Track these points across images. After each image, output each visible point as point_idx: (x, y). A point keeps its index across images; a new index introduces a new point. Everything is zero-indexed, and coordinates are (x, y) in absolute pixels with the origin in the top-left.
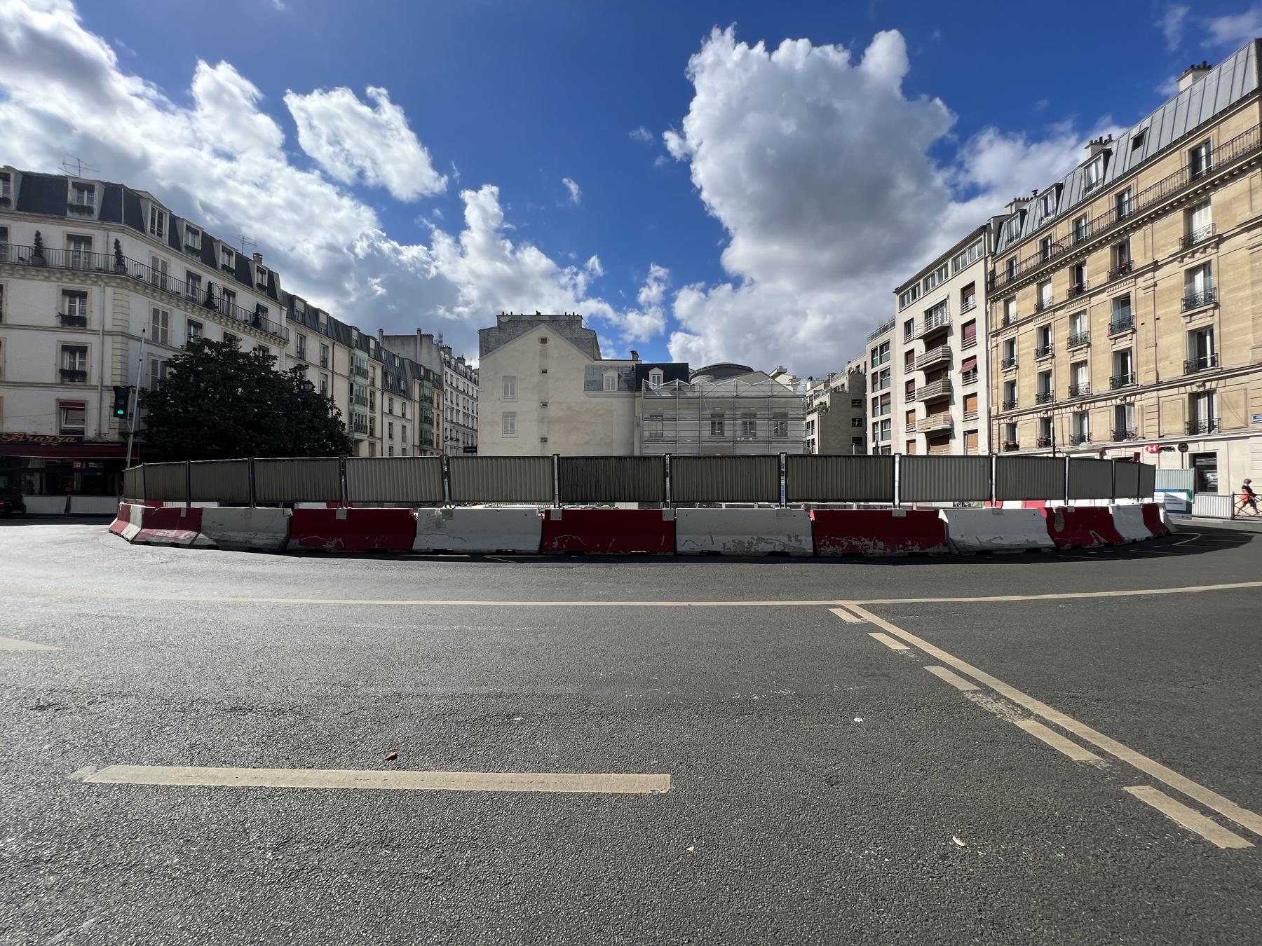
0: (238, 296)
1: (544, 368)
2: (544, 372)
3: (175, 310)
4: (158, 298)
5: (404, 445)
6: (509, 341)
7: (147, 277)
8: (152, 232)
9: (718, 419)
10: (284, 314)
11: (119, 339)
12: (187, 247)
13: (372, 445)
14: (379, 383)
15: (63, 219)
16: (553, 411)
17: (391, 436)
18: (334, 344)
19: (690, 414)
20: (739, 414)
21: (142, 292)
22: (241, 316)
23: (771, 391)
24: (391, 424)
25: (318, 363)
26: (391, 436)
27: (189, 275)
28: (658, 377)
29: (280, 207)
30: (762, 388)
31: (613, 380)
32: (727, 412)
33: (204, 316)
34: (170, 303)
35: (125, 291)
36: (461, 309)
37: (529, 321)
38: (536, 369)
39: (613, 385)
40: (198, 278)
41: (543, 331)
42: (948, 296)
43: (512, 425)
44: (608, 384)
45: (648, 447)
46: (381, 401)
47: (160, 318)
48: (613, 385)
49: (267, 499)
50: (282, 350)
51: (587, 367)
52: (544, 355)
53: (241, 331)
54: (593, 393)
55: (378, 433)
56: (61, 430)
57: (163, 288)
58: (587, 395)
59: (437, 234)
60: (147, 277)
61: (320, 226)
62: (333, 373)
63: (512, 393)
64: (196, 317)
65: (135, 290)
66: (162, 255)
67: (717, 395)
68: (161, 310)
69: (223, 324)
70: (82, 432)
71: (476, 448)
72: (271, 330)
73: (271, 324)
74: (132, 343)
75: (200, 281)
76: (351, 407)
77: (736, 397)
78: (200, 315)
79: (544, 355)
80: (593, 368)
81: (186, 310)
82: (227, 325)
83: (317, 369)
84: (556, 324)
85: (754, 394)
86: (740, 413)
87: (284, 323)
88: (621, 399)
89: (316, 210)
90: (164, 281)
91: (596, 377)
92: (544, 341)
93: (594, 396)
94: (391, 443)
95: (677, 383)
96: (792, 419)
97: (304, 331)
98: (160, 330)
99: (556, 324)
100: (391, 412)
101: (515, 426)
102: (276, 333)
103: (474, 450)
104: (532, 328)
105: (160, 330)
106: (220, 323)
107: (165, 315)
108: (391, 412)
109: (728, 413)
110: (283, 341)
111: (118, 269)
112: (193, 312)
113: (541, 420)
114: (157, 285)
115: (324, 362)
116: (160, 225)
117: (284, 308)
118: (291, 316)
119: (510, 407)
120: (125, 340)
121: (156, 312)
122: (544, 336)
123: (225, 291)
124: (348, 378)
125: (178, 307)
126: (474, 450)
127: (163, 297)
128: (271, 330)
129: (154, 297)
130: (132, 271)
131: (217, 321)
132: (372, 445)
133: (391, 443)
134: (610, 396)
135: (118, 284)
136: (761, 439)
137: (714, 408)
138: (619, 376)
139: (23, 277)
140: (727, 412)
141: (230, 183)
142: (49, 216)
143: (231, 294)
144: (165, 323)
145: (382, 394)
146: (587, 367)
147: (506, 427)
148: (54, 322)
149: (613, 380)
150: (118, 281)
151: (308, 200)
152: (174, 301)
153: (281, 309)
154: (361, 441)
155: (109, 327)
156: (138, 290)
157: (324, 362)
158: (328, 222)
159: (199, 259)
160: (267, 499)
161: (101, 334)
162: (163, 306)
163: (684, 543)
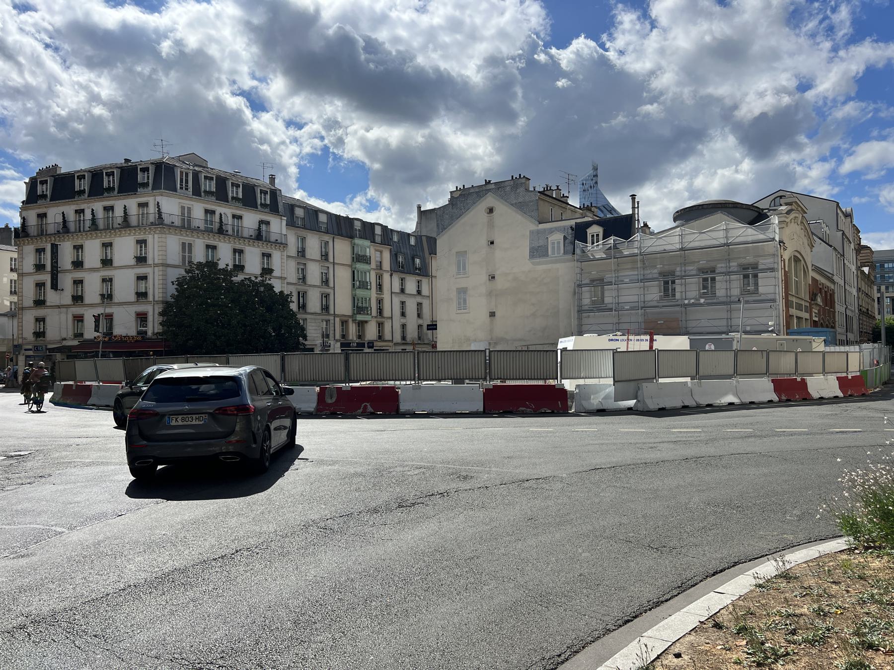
0: (244, 218)
1: (491, 240)
2: (492, 243)
3: (197, 240)
4: (184, 235)
5: (420, 322)
6: (461, 216)
7: (178, 222)
8: (181, 188)
9: (670, 279)
10: (284, 223)
11: (161, 268)
12: (205, 192)
13: (380, 325)
14: (386, 265)
15: (136, 194)
16: (501, 283)
17: (403, 314)
18: (334, 238)
19: (628, 274)
20: (693, 269)
21: (173, 233)
22: (246, 234)
23: (726, 237)
24: (403, 303)
25: (318, 257)
26: (403, 314)
27: (207, 211)
28: (598, 235)
29: (441, 27)
30: (714, 235)
31: (559, 243)
32: (719, 266)
33: (217, 240)
34: (192, 236)
35: (164, 236)
36: (649, 108)
37: (477, 192)
38: (484, 242)
39: (559, 248)
40: (213, 212)
41: (490, 200)
42: (595, 169)
43: (465, 300)
44: (553, 248)
45: (589, 317)
46: (391, 283)
47: (187, 248)
48: (559, 248)
49: (304, 380)
50: (283, 253)
51: (532, 232)
52: (491, 225)
53: (247, 245)
54: (538, 260)
55: (387, 312)
56: (138, 332)
57: (189, 228)
58: (533, 264)
59: (611, 14)
60: (178, 222)
61: (482, 39)
62: (334, 263)
63: (464, 269)
64: (212, 242)
65: (170, 233)
66: (187, 203)
67: (658, 249)
68: (187, 243)
69: (232, 242)
70: (146, 332)
71: (436, 325)
72: (273, 239)
73: (272, 234)
74: (169, 270)
75: (215, 214)
76: (354, 292)
77: (682, 249)
78: (215, 240)
79: (491, 225)
80: (538, 232)
81: (204, 238)
82: (235, 243)
83: (317, 264)
84: (501, 192)
85: (703, 244)
86: (735, 264)
87: (284, 231)
88: (568, 264)
89: (478, 21)
90: (189, 222)
91: (541, 243)
92: (491, 210)
93: (539, 264)
94: (403, 321)
95: (612, 241)
96: (764, 270)
97: (303, 233)
98: (187, 257)
99: (501, 192)
100: (402, 291)
101: (467, 302)
102: (277, 240)
103: (435, 327)
104: (480, 199)
105: (187, 257)
106: (230, 242)
107: (190, 245)
108: (402, 291)
109: (721, 267)
110: (282, 246)
111: (160, 222)
112: (209, 239)
113: (490, 294)
114: (186, 226)
115: (325, 256)
116: (187, 182)
117: (283, 218)
118: (291, 224)
119: (463, 283)
120: (164, 268)
121: (184, 244)
122: (491, 205)
123: (234, 216)
124: (351, 266)
125: (198, 237)
126: (435, 327)
127: (188, 233)
128: (273, 239)
129: (182, 235)
130: (167, 220)
131: (228, 241)
132: (380, 325)
133: (403, 321)
134: (556, 262)
135: (160, 231)
136: (722, 299)
137: (590, 273)
138: (565, 238)
139: (120, 236)
140: (719, 266)
141: (394, 14)
142: (130, 193)
143: (240, 217)
144: (190, 251)
145: (391, 275)
146: (532, 232)
147: (459, 303)
148: (133, 262)
149: (559, 243)
150: (159, 229)
151: (468, 12)
152: (195, 234)
153: (281, 219)
154: (366, 322)
155: (156, 261)
156: (177, 233)
157: (325, 256)
158: (490, 32)
159: (214, 198)
160: (304, 380)
161: (152, 266)
162: (188, 239)
163: (403, 407)
